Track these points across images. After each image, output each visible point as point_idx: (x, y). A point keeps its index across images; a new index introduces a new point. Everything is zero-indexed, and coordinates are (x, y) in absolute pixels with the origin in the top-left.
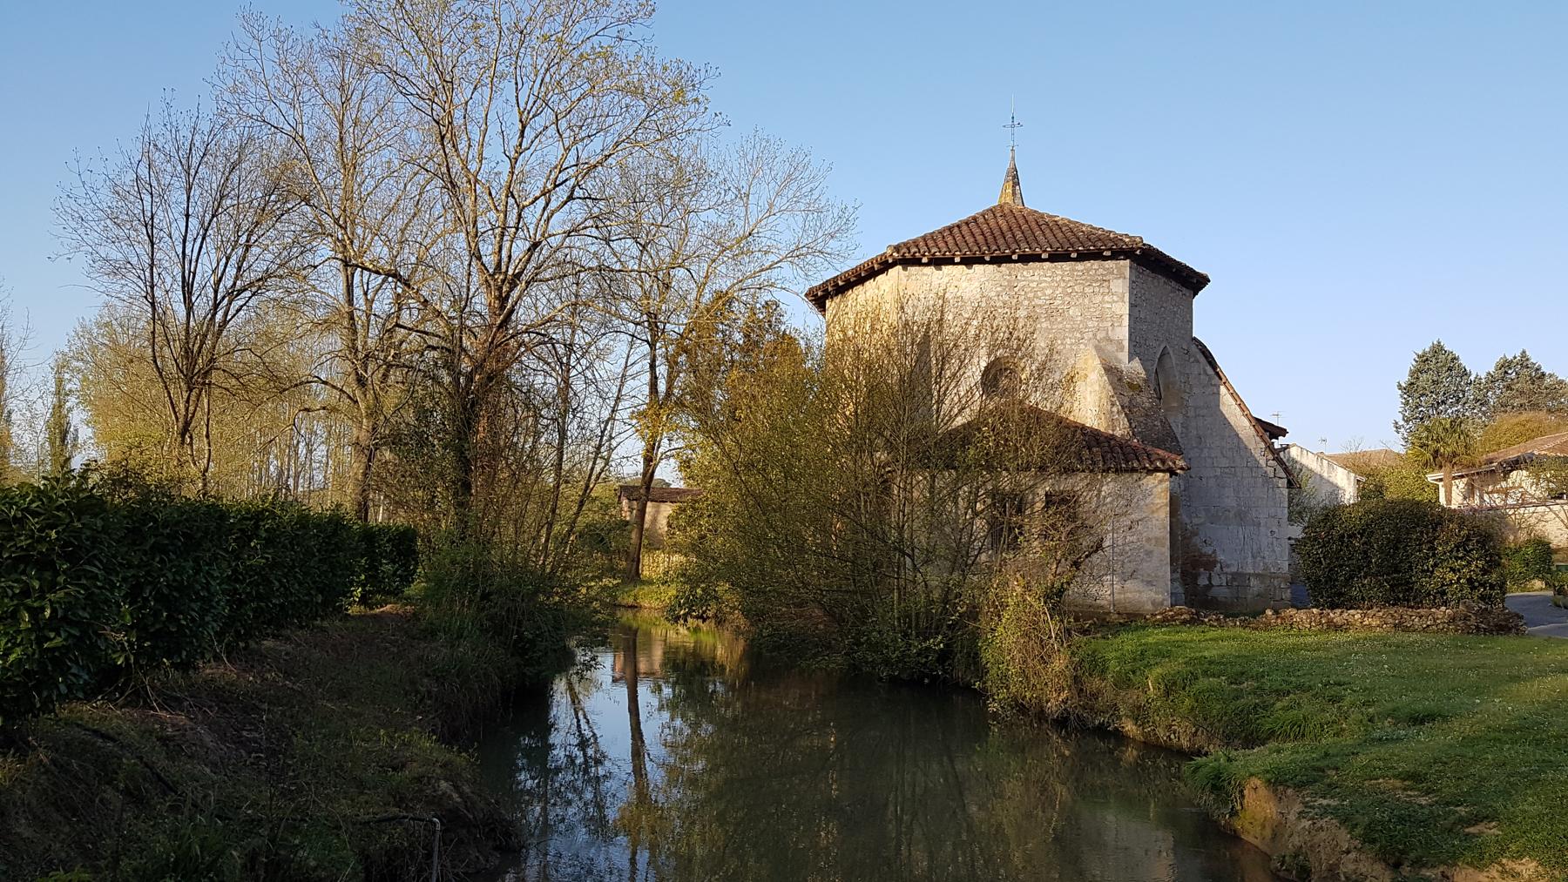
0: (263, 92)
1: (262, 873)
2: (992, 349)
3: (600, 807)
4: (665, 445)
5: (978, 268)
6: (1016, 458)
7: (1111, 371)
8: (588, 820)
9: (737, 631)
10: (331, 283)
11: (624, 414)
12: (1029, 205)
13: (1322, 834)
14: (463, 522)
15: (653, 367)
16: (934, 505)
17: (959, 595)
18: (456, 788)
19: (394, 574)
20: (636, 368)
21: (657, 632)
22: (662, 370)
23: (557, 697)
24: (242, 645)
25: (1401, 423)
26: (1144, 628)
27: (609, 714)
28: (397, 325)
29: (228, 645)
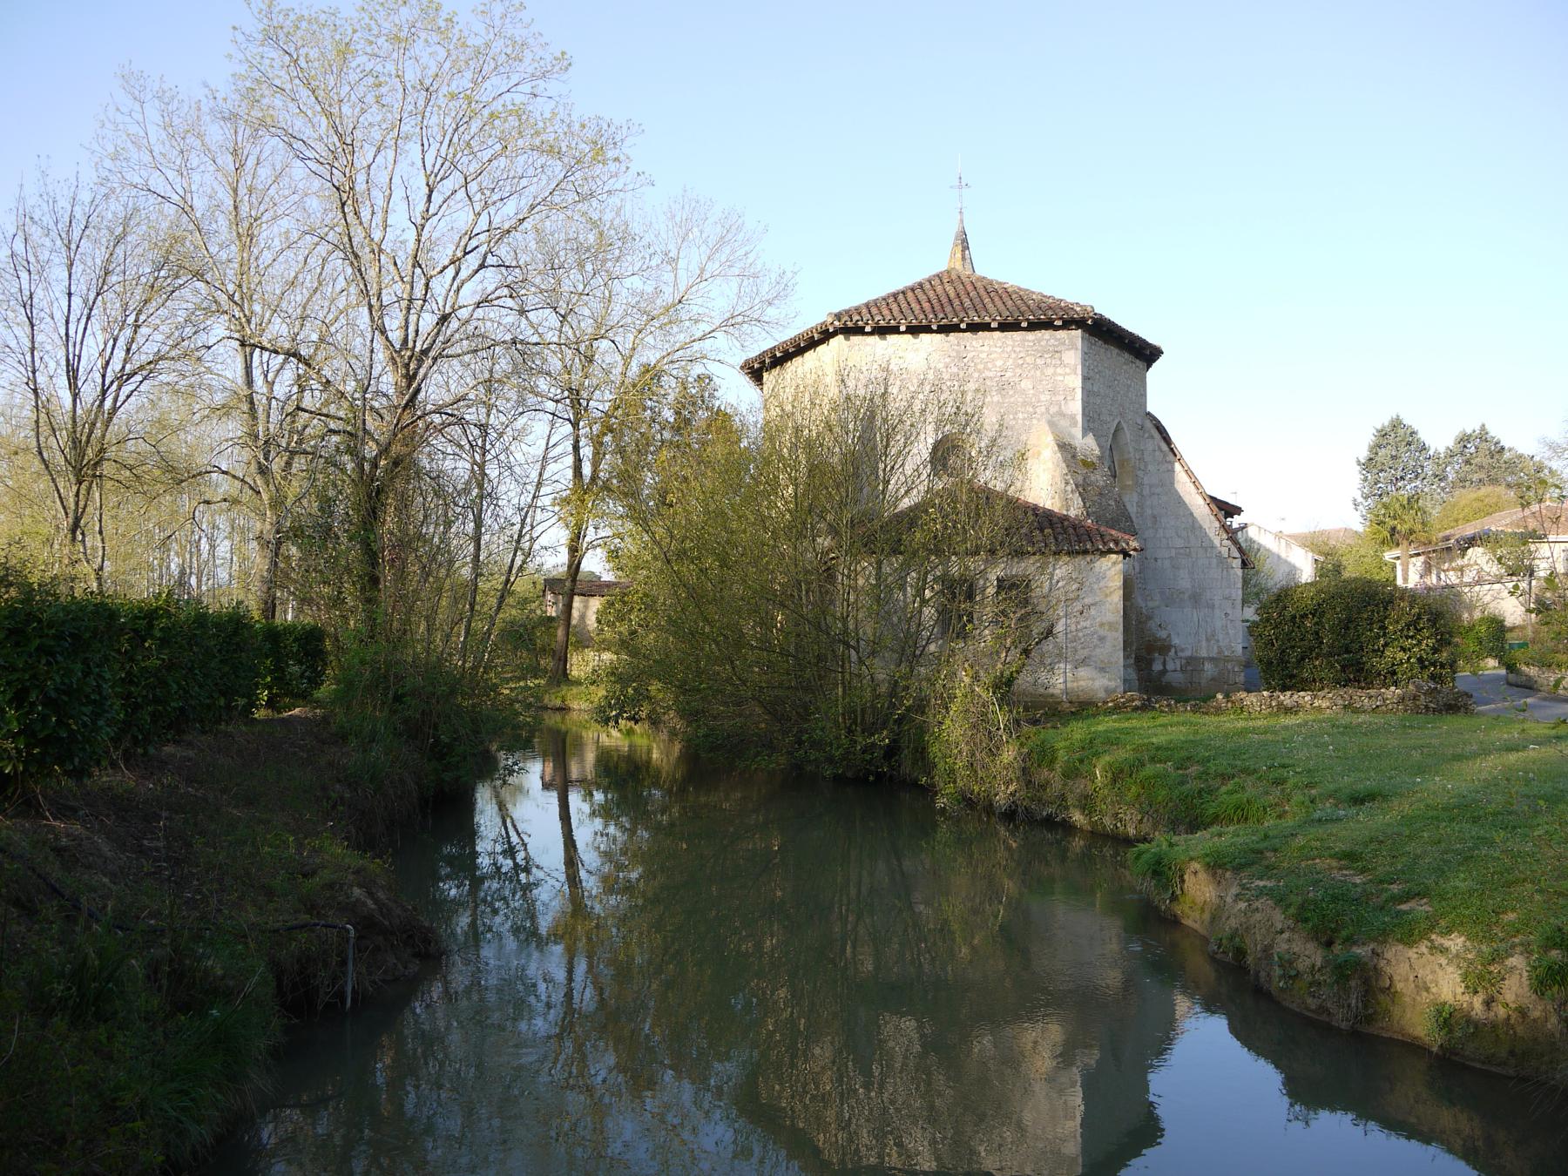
0: (147, 158)
1: (165, 982)
2: (939, 424)
3: (532, 915)
4: (591, 535)
6: (964, 541)
7: (1064, 447)
8: (516, 930)
9: (673, 733)
10: (227, 365)
11: (545, 501)
12: (980, 272)
13: (1258, 916)
14: (371, 619)
15: (576, 448)
16: (881, 594)
17: (907, 688)
18: (370, 894)
19: (302, 676)
21: (589, 735)
22: (587, 451)
23: (480, 804)
24: (140, 751)
25: (1360, 499)
26: (1094, 716)
27: (538, 823)
28: (299, 408)
29: (126, 751)
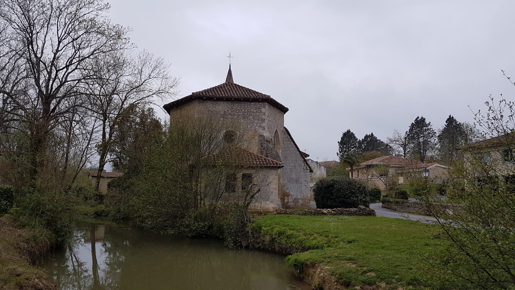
15: (104, 129)
20: (97, 129)
22: (108, 130)
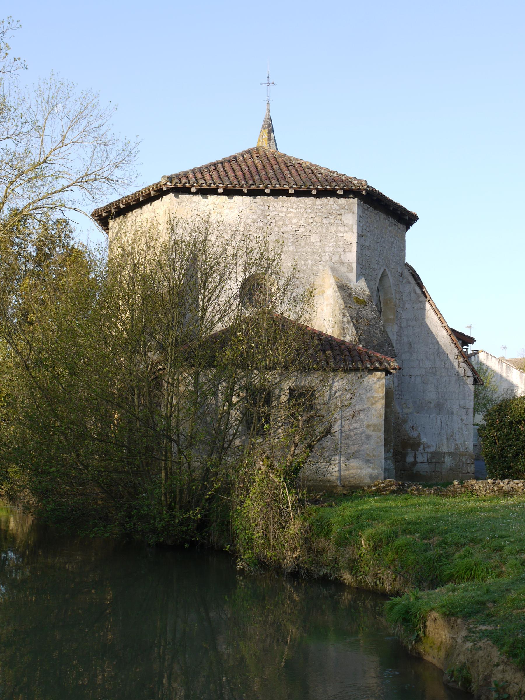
2: (247, 267)
5: (237, 199)
6: (264, 358)
7: (343, 288)
9: (27, 508)
13: (481, 653)
16: (198, 398)
26: (361, 497)
